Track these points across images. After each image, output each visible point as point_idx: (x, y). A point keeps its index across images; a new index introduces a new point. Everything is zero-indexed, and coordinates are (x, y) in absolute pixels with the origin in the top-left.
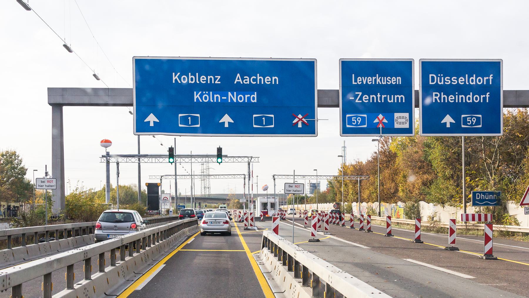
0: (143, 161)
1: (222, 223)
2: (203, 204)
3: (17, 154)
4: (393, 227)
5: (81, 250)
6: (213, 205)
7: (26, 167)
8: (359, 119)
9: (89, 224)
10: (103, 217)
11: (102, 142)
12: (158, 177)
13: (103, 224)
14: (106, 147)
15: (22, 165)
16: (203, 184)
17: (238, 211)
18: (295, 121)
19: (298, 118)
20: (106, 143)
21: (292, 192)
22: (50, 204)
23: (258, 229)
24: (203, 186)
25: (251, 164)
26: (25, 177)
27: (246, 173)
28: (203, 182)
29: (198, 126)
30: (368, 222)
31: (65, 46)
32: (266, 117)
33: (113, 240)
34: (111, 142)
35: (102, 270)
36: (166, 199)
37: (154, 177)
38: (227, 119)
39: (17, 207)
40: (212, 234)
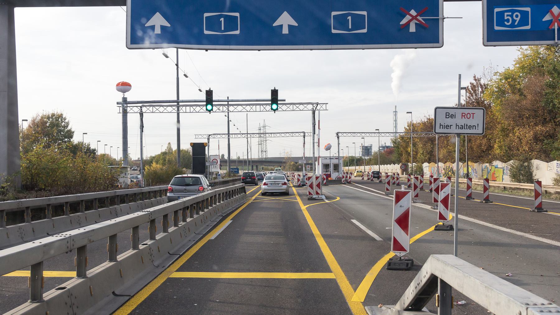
3: (64, 116)
4: (490, 192)
5: (63, 237)
6: (270, 168)
7: (73, 130)
8: (517, 16)
9: (163, 187)
10: (175, 181)
11: (118, 85)
12: (205, 136)
14: (124, 92)
15: (69, 128)
17: (296, 173)
18: (404, 22)
19: (411, 15)
20: (124, 87)
21: (454, 130)
23: (327, 198)
25: (317, 112)
26: (72, 140)
27: (308, 128)
29: (237, 32)
30: (398, 179)
32: (353, 16)
34: (130, 85)
35: (165, 230)
36: (214, 162)
37: (200, 137)
38: (285, 21)
40: (272, 194)
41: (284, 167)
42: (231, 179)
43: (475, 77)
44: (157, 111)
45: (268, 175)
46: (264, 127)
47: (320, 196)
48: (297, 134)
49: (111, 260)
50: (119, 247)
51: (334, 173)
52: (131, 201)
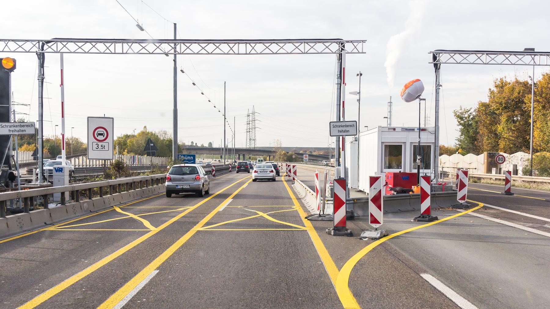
0: (50, 50)
1: (268, 172)
2: (247, 157)
13: (172, 176)
16: (248, 136)
22: (491, 132)
24: (248, 138)
28: (248, 133)
31: (138, 26)
41: (274, 157)
44: (80, 50)
46: (253, 113)
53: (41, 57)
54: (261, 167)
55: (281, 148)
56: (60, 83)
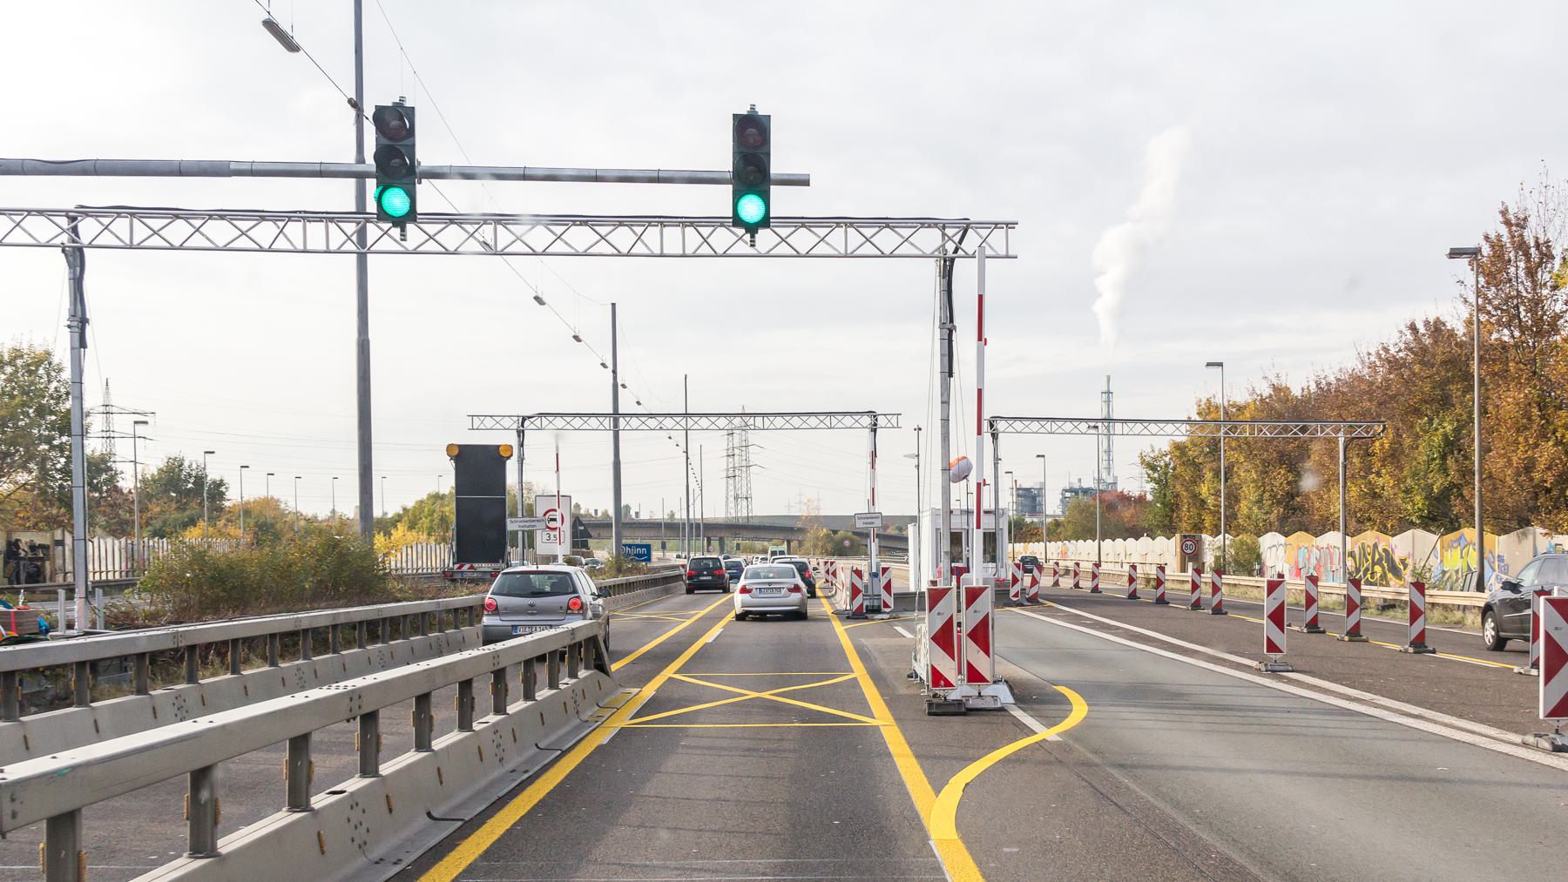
3: (55, 360)
4: (1432, 623)
5: (341, 690)
6: (758, 545)
10: (502, 585)
12: (507, 422)
24: (732, 493)
28: (731, 481)
33: (529, 638)
37: (489, 422)
39: (42, 547)
40: (762, 617)
42: (621, 579)
43: (1504, 213)
44: (156, 241)
45: (758, 565)
47: (989, 690)
48: (848, 420)
49: (365, 773)
50: (386, 740)
51: (1000, 563)
52: (349, 644)
53: (76, 257)
54: (763, 573)
55: (817, 518)
56: (88, 329)
